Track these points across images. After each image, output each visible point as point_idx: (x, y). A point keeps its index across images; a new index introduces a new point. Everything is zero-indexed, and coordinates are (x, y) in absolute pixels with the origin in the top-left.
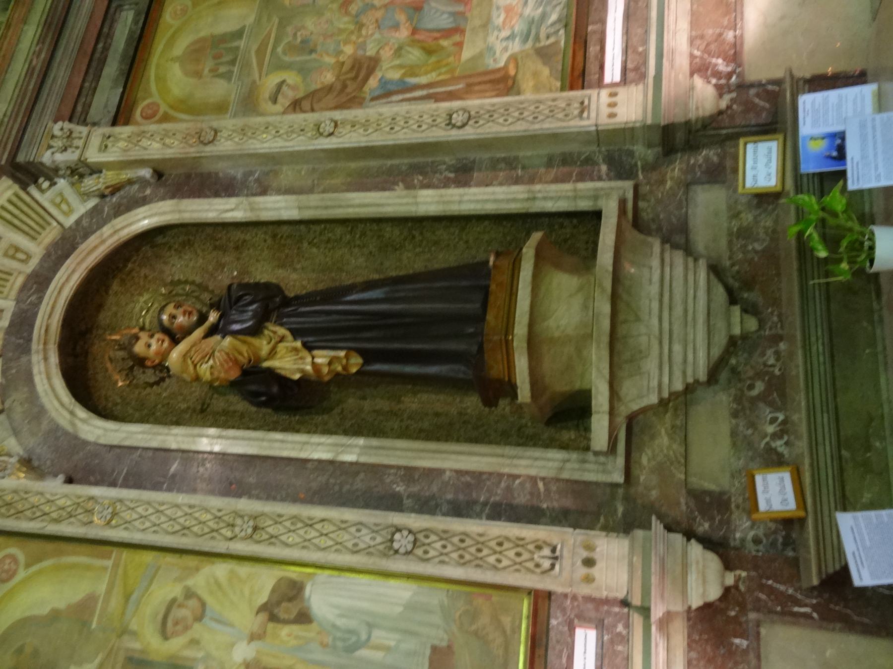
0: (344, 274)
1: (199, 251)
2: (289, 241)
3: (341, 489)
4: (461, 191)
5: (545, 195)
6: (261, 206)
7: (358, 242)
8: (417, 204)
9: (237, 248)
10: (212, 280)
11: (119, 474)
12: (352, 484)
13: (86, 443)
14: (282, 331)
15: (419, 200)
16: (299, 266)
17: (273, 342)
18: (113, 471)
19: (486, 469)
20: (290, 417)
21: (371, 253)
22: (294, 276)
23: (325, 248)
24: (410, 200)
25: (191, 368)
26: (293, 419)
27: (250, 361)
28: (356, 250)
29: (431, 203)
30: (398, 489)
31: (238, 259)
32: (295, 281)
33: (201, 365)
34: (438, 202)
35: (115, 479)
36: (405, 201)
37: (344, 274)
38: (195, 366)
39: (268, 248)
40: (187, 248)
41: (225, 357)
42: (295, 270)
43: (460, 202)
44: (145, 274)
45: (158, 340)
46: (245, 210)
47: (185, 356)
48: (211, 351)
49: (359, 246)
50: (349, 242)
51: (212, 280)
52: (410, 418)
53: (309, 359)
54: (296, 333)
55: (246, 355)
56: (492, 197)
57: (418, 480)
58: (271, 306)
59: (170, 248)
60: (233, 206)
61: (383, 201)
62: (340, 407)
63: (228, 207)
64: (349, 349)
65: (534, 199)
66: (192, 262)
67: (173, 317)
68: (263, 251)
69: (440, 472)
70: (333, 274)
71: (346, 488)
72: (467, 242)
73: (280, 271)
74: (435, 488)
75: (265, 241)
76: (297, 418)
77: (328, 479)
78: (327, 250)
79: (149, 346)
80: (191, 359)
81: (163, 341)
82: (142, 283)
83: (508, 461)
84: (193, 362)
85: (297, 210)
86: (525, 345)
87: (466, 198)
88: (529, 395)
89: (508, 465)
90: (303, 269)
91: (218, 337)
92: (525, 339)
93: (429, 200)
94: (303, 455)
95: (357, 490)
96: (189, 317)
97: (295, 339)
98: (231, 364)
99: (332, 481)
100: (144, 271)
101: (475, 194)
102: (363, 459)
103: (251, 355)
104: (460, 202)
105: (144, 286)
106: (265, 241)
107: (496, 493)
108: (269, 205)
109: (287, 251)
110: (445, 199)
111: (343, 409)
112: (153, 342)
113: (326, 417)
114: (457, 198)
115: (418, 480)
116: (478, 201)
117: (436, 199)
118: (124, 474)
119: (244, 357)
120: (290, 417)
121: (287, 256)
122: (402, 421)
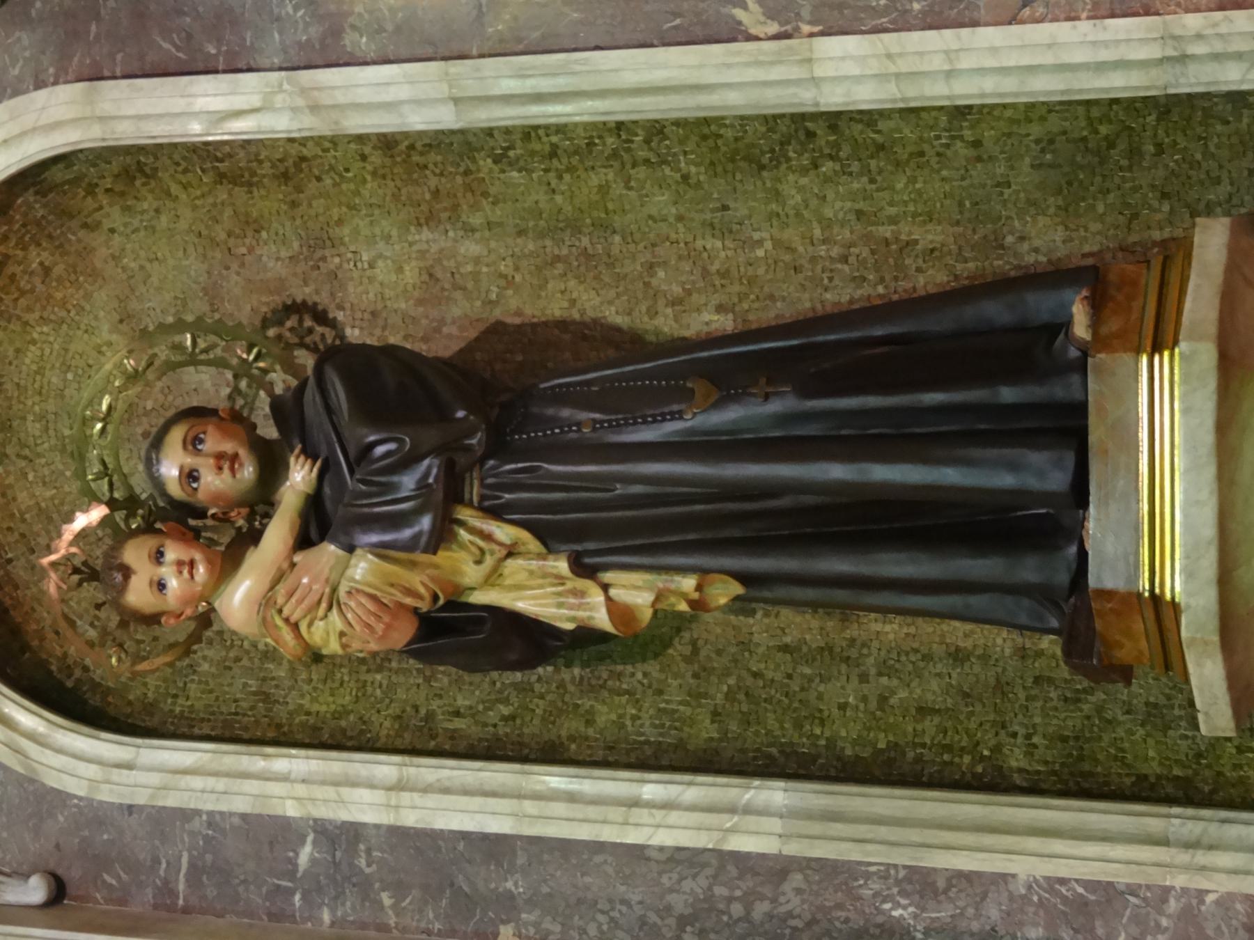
0: (617, 238)
1: (175, 189)
2: (434, 157)
3: (748, 908)
4: (947, 38)
5: (1219, 47)
6: (341, 98)
7: (642, 154)
8: (815, 81)
9: (285, 177)
10: (235, 266)
11: (174, 866)
12: (774, 901)
13: (62, 797)
14: (504, 532)
15: (819, 72)
16: (476, 220)
17: (489, 561)
18: (156, 861)
19: (1122, 876)
20: (557, 670)
21: (685, 178)
22: (471, 248)
23: (546, 171)
24: (796, 72)
25: (287, 635)
26: (566, 675)
27: (435, 598)
28: (641, 172)
29: (858, 79)
30: (896, 913)
31: (294, 204)
32: (477, 261)
33: (310, 625)
34: (881, 77)
35: (166, 882)
36: (776, 74)
37: (617, 238)
38: (295, 627)
39: (374, 174)
40: (138, 183)
41: (370, 606)
42: (470, 230)
43: (950, 74)
44: (41, 264)
45: (180, 563)
46: (294, 110)
47: (266, 602)
48: (327, 590)
49: (647, 162)
50: (615, 154)
51: (235, 266)
52: (885, 669)
53: (597, 597)
54: (549, 537)
55: (422, 590)
56: (1048, 59)
57: (945, 892)
58: (462, 460)
59: (91, 190)
60: (256, 101)
61: (710, 77)
62: (686, 635)
63: (239, 102)
64: (703, 572)
65: (1183, 59)
66: (164, 219)
67: (190, 476)
68: (364, 181)
69: (1005, 878)
70: (585, 241)
71: (761, 909)
72: (977, 144)
73: (426, 234)
74: (993, 913)
75: (364, 158)
76: (577, 671)
77: (710, 888)
78: (552, 175)
79: (161, 586)
80: (280, 611)
81: (192, 564)
82: (40, 288)
83: (1183, 857)
84: (287, 620)
85: (451, 106)
86: (1216, 638)
87: (965, 63)
88: (1232, 725)
89: (1186, 868)
90: (490, 225)
91: (329, 551)
92: (1213, 624)
93: (853, 69)
94: (633, 837)
95: (790, 915)
96: (233, 471)
97: (551, 550)
98: (387, 619)
99: (720, 891)
100: (37, 257)
101: (994, 50)
102: (793, 849)
103: (431, 585)
104: (950, 74)
105: (49, 297)
106: (364, 158)
107: (1158, 925)
108: (364, 96)
109: (433, 182)
110: (903, 66)
111: (694, 643)
112: (167, 572)
113: (653, 667)
114: (938, 63)
115: (945, 892)
116: (1004, 71)
117: (874, 67)
118: (183, 871)
119: (420, 597)
120: (557, 670)
121: (436, 193)
122: (864, 678)
